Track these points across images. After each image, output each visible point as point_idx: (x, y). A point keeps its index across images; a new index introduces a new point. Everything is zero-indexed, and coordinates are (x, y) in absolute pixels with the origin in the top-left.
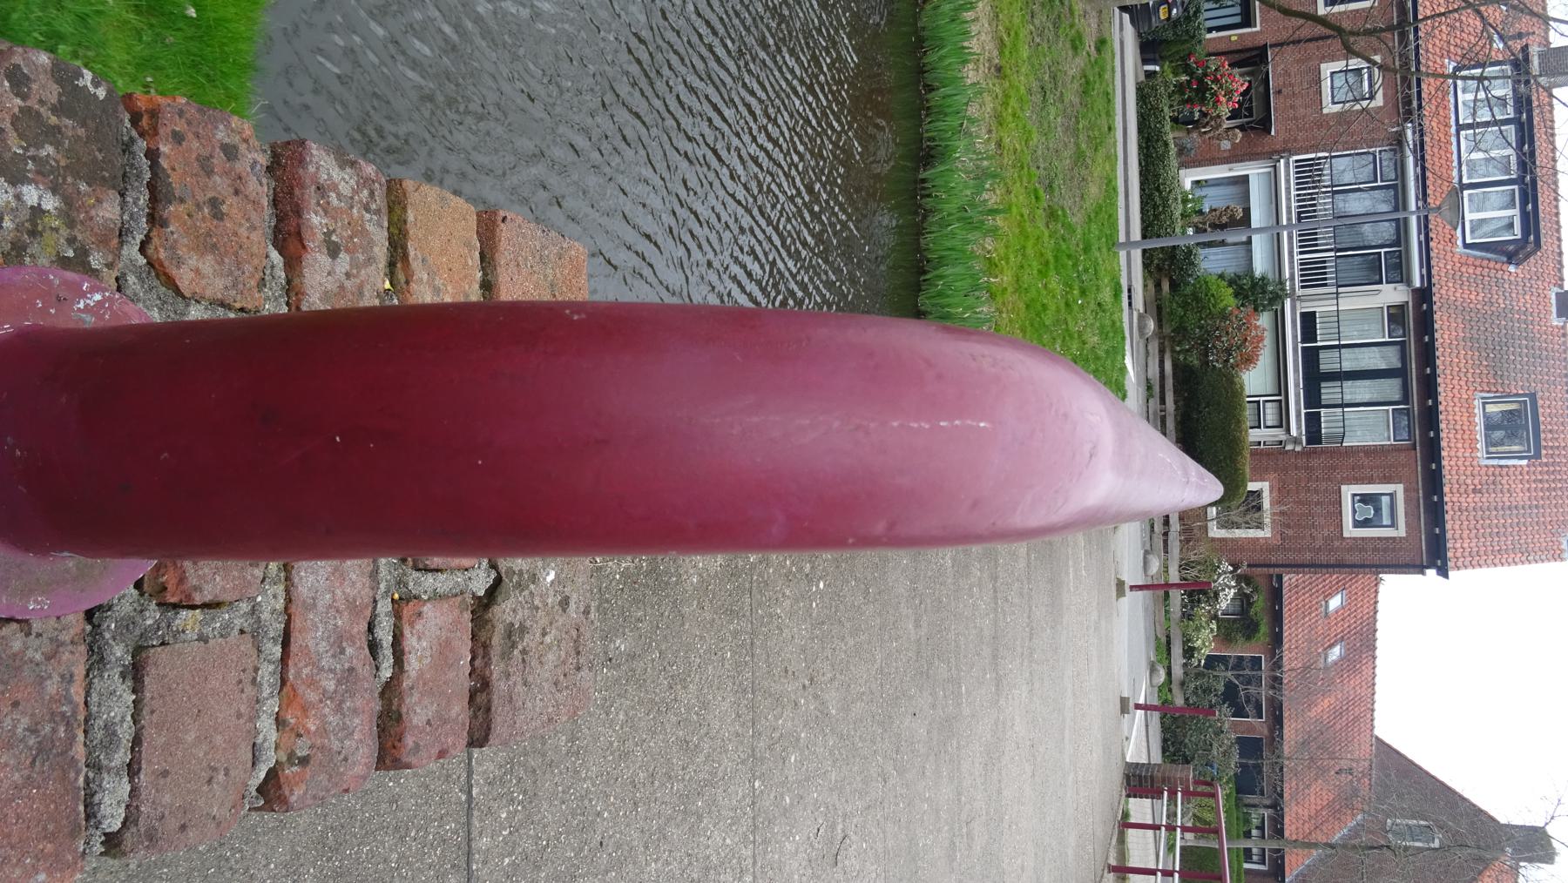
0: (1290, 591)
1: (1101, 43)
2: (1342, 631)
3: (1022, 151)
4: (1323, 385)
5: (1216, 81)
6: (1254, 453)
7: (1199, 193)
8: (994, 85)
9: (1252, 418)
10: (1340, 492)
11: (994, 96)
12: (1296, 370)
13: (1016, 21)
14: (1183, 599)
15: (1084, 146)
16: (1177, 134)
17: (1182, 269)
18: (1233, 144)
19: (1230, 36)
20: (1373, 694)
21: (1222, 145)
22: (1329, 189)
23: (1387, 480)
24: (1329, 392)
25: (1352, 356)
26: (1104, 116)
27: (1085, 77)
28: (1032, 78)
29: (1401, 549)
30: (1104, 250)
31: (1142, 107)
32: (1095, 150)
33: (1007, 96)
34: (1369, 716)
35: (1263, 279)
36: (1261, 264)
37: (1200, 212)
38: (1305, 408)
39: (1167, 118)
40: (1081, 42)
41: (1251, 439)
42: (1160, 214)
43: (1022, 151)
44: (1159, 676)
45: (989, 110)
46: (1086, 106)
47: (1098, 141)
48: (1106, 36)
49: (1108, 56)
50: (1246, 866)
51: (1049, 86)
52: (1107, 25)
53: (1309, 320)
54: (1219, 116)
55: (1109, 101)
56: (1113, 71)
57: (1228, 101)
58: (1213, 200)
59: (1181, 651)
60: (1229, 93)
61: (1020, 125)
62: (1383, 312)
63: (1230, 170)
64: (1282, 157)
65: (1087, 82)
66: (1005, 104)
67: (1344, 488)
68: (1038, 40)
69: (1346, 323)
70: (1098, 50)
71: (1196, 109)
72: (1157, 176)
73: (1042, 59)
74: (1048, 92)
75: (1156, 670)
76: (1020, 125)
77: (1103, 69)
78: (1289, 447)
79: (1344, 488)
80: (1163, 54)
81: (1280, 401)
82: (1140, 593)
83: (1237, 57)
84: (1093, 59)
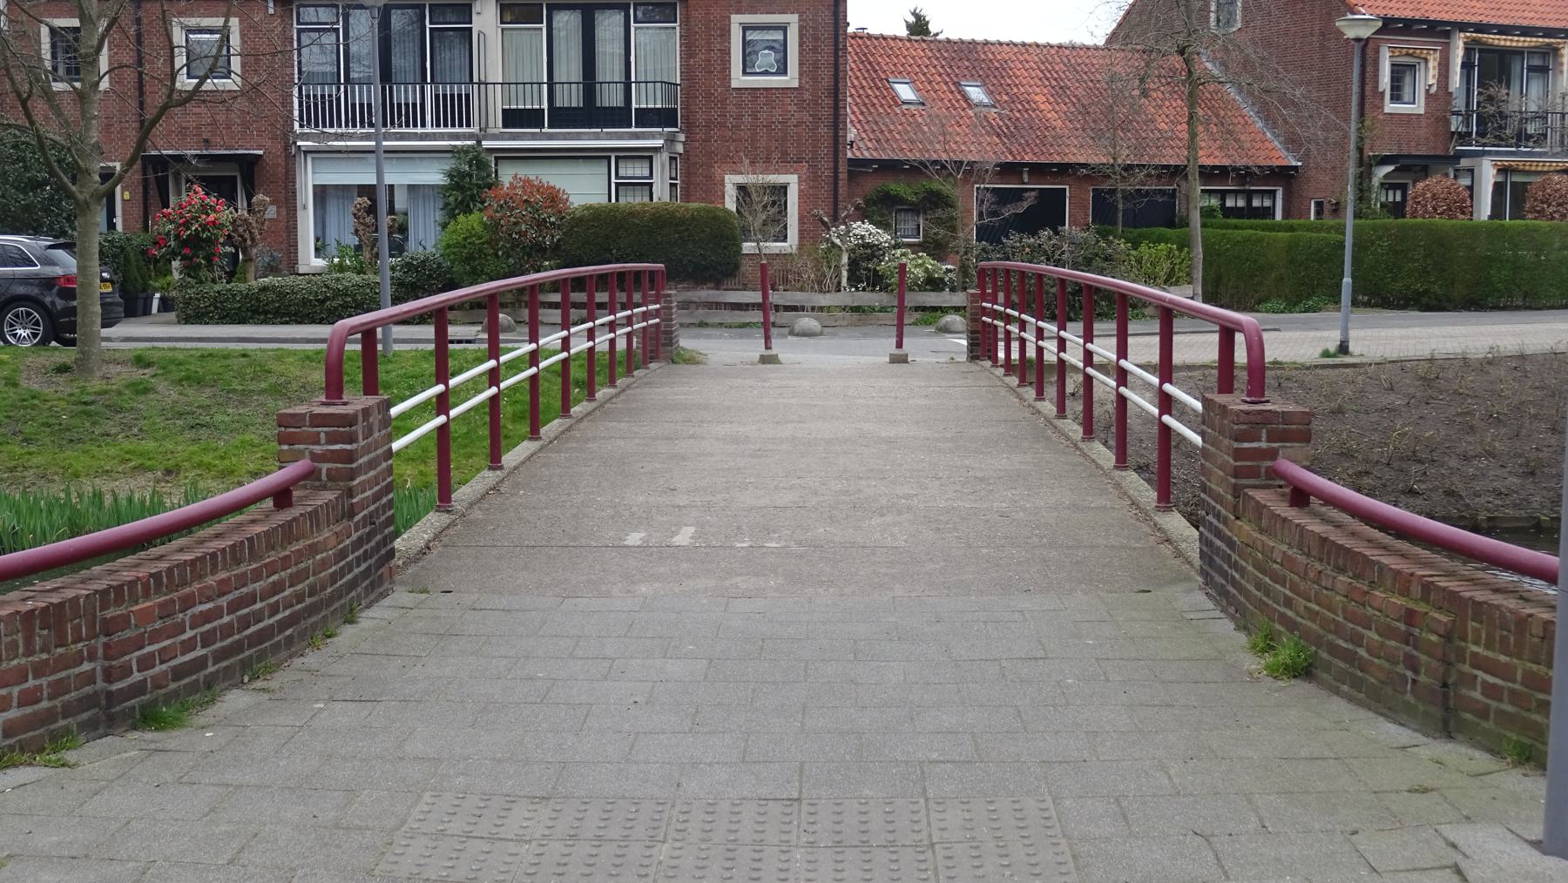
0: (884, 150)
1: (140, 361)
2: (946, 83)
3: (264, 451)
4: (598, 105)
5: (187, 225)
6: (687, 196)
7: (332, 248)
8: (186, 477)
9: (638, 193)
10: (741, 89)
11: (198, 478)
12: (578, 137)
13: (112, 451)
14: (864, 290)
15: (263, 385)
16: (251, 275)
17: (430, 276)
18: (272, 203)
19: (123, 200)
20: (1038, 46)
21: (270, 216)
22: (342, 87)
23: (725, 33)
24: (610, 97)
25: (564, 68)
26: (229, 362)
27: (181, 380)
28: (180, 438)
29: (814, 21)
30: (390, 367)
31: (212, 318)
32: (270, 372)
33: (200, 465)
34: (1067, 52)
35: (450, 176)
36: (433, 175)
37: (358, 248)
38: (630, 126)
39: (229, 286)
40: (141, 383)
41: (667, 199)
42: (355, 300)
43: (264, 451)
44: (954, 322)
45: (214, 484)
46: (215, 381)
47: (258, 368)
48: (131, 355)
49: (156, 355)
50: (1279, 216)
51: (191, 421)
52: (117, 355)
53: (513, 118)
54: (234, 222)
55: (210, 355)
56: (175, 349)
57: (215, 211)
58: (343, 230)
59: (932, 294)
60: (205, 209)
61: (236, 452)
62: (507, 29)
63: (305, 207)
64: (295, 143)
65: (188, 378)
66: (209, 467)
67: (734, 84)
68: (135, 430)
69: (520, 75)
70: (149, 365)
71: (222, 250)
72: (305, 302)
73: (157, 427)
74: (197, 421)
75: (945, 326)
76: (236, 452)
77: (172, 361)
78: (680, 148)
79: (734, 84)
80: (140, 288)
81: (617, 158)
82: (905, 340)
83: (154, 193)
84: (159, 372)
